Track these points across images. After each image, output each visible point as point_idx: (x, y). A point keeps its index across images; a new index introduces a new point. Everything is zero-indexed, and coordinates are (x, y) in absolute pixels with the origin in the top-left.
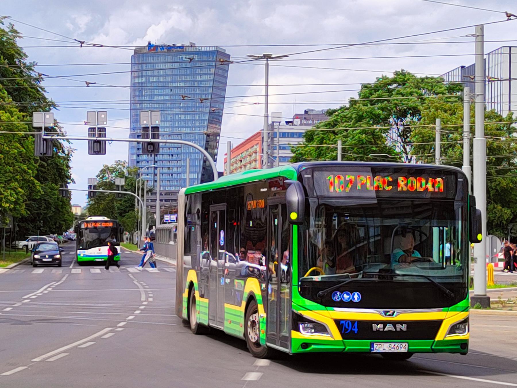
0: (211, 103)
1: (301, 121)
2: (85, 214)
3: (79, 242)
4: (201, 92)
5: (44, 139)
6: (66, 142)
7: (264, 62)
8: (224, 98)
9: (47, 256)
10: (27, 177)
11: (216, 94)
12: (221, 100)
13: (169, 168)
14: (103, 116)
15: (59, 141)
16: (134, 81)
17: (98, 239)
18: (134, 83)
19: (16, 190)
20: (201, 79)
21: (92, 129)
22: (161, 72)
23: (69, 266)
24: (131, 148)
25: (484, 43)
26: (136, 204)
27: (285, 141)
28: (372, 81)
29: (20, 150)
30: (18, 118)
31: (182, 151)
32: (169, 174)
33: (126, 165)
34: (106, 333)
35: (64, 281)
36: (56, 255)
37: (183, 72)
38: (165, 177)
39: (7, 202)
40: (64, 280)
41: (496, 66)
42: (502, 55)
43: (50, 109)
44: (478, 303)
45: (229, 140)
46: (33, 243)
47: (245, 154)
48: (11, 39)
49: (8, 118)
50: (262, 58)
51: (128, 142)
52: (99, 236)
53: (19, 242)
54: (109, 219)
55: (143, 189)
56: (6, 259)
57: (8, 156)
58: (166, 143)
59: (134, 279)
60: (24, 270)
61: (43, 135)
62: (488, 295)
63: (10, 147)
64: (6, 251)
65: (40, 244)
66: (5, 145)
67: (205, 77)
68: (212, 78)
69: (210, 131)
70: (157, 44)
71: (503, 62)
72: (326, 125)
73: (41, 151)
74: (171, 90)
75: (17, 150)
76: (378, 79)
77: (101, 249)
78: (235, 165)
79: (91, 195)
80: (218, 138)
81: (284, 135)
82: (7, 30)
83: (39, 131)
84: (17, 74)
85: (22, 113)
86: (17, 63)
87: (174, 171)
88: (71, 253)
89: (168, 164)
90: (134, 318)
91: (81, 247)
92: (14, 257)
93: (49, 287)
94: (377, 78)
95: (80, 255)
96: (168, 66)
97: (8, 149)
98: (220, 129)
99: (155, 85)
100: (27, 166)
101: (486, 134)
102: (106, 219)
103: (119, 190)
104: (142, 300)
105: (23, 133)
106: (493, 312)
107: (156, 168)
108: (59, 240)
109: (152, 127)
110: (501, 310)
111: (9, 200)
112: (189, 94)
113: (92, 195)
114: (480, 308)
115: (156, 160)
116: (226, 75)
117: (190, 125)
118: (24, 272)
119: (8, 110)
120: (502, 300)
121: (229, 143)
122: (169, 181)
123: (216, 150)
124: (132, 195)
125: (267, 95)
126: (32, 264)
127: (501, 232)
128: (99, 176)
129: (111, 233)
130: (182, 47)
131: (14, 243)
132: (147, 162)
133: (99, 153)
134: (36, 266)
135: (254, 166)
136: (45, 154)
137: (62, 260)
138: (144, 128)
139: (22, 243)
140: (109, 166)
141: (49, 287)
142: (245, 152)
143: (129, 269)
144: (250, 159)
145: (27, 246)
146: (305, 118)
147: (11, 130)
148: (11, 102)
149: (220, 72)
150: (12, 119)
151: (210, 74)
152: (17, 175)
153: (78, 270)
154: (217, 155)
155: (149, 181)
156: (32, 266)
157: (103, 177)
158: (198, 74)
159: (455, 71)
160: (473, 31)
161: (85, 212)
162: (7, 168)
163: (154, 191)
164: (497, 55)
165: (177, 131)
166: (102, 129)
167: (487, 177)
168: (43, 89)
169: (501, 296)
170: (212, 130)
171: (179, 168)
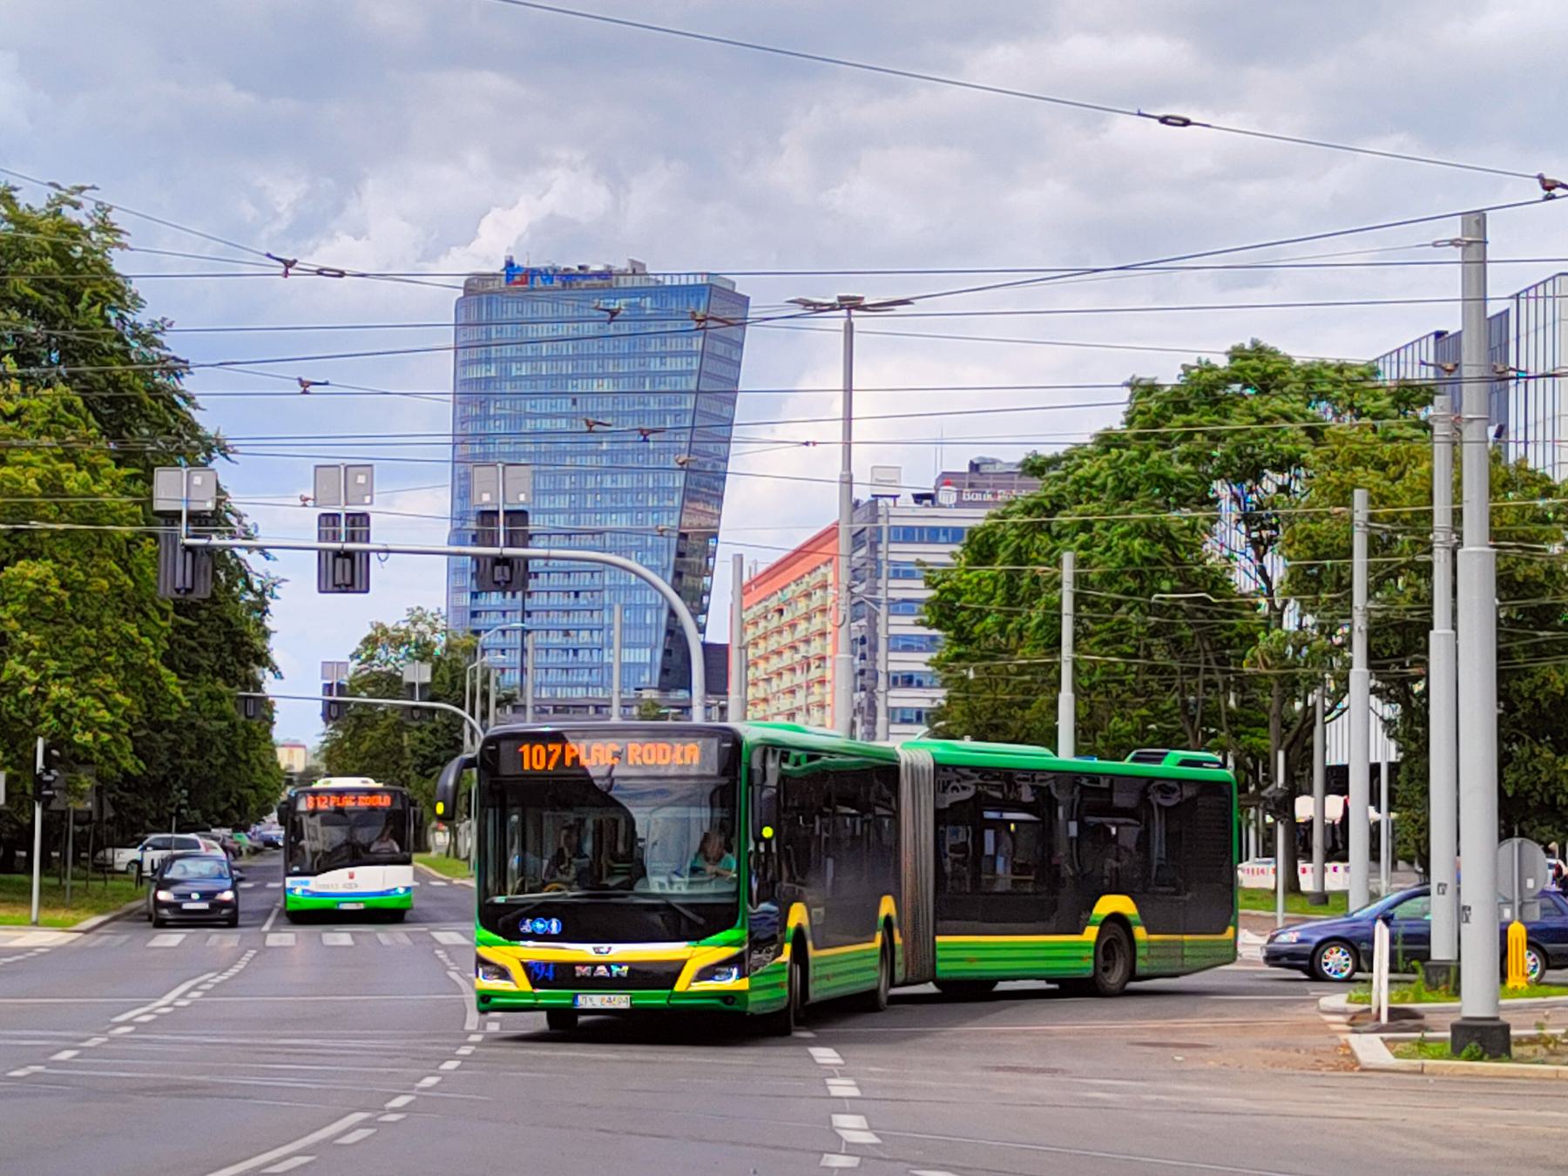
0: (691, 442)
1: (960, 493)
2: (317, 767)
3: (293, 850)
4: (662, 407)
5: (189, 548)
6: (256, 553)
7: (837, 320)
8: (731, 425)
9: (195, 896)
10: (137, 658)
11: (707, 415)
12: (721, 432)
13: (567, 633)
14: (361, 479)
15: (237, 551)
16: (465, 373)
17: (347, 843)
18: (467, 382)
19: (106, 697)
20: (663, 369)
21: (329, 520)
22: (545, 349)
23: (262, 925)
24: (453, 572)
25: (1488, 265)
26: (467, 741)
27: (906, 553)
28: (1169, 376)
29: (118, 583)
30: (113, 483)
31: (607, 582)
32: (567, 650)
33: (440, 625)
34: (349, 1128)
35: (241, 971)
36: (222, 891)
37: (609, 345)
38: (554, 658)
39: (85, 729)
40: (240, 966)
41: (1541, 333)
42: (1557, 300)
43: (210, 459)
44: (1473, 1044)
45: (738, 550)
46: (157, 855)
47: (794, 591)
48: (97, 252)
49: (85, 486)
50: (832, 307)
51: (445, 557)
52: (351, 833)
53: (117, 851)
54: (380, 785)
55: (485, 696)
56: (75, 905)
57: (84, 598)
58: (548, 558)
59: (449, 964)
60: (124, 938)
61: (184, 534)
62: (1505, 1017)
63: (88, 569)
64: (74, 878)
65: (174, 858)
66: (76, 564)
67: (673, 364)
68: (695, 367)
69: (691, 522)
70: (533, 265)
71: (1560, 320)
72: (1028, 511)
73: (179, 584)
74: (574, 402)
75: (110, 583)
76: (1186, 369)
77: (356, 876)
78: (762, 623)
79: (333, 712)
80: (712, 543)
81: (908, 535)
82: (88, 225)
83: (173, 525)
84: (111, 355)
85: (124, 472)
86: (113, 323)
87: (581, 640)
88: (271, 885)
89: (564, 620)
90: (439, 1083)
91: (296, 869)
92: (98, 897)
93: (194, 988)
94: (1183, 366)
95: (292, 890)
96: (564, 330)
97: (82, 578)
98: (719, 517)
99: (527, 387)
100: (139, 627)
101: (1495, 536)
102: (371, 783)
103: (412, 699)
104: (468, 1027)
105: (126, 530)
106: (1518, 1070)
107: (525, 632)
108: (236, 846)
109: (506, 513)
110: (1543, 1063)
111: (92, 719)
112: (607, 414)
113: (334, 714)
114: (1480, 1058)
115: (527, 608)
116: (735, 358)
117: (629, 505)
118: (128, 941)
119: (86, 463)
120: (1548, 1032)
121: (737, 559)
122: (567, 669)
123: (706, 580)
124: (455, 715)
125: (848, 419)
126: (150, 919)
127: (1554, 827)
128: (358, 657)
129: (387, 824)
130: (606, 275)
131: (101, 854)
132: (500, 614)
133: (350, 589)
134: (161, 924)
135: (819, 627)
136: (189, 591)
137: (241, 908)
138: (483, 513)
139: (124, 857)
140: (389, 625)
141: (194, 988)
142: (793, 586)
143: (439, 936)
144: (808, 606)
145: (139, 863)
146: (971, 485)
147: (90, 521)
148: (94, 439)
149: (720, 348)
150: (97, 489)
151: (691, 354)
152: (109, 654)
153: (287, 938)
154: (709, 593)
155: (507, 671)
156: (151, 924)
157: (371, 657)
158: (655, 355)
159: (1417, 345)
160: (1454, 230)
161: (314, 762)
162: (78, 632)
163: (521, 702)
164: (1532, 301)
165: (588, 522)
166: (358, 519)
167: (1498, 665)
168: (188, 399)
169: (1544, 1021)
170: (695, 522)
171: (595, 633)
